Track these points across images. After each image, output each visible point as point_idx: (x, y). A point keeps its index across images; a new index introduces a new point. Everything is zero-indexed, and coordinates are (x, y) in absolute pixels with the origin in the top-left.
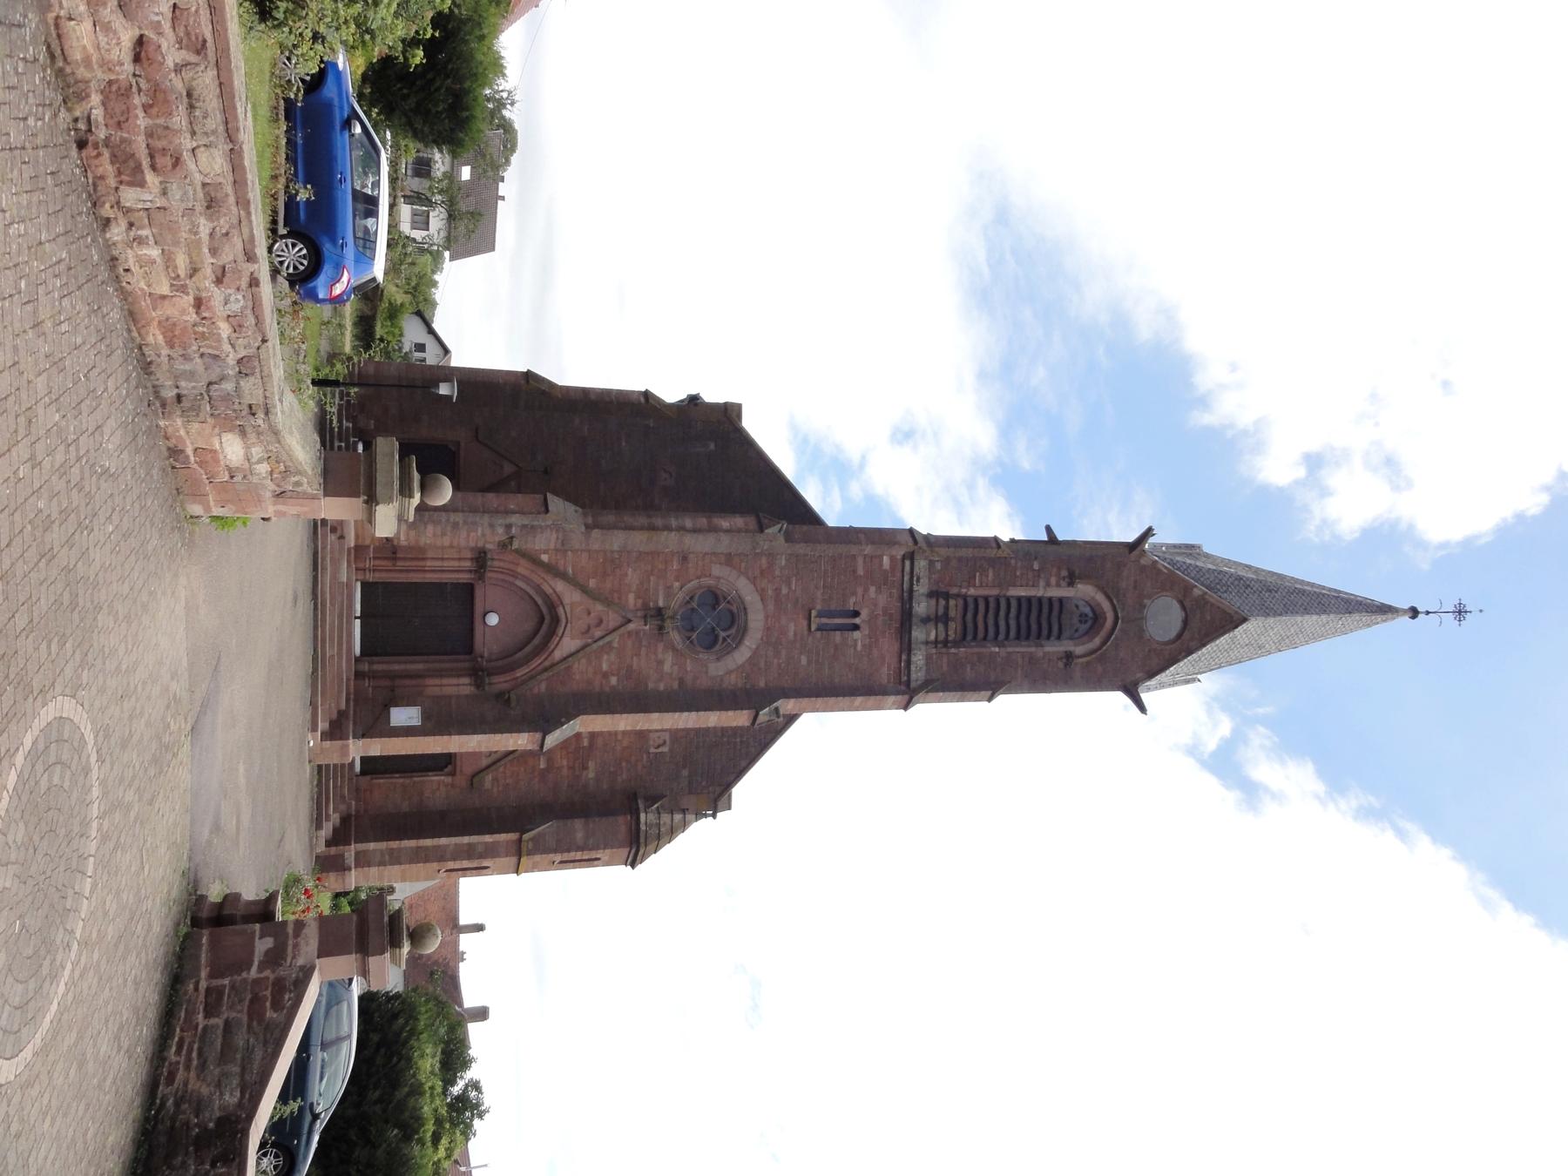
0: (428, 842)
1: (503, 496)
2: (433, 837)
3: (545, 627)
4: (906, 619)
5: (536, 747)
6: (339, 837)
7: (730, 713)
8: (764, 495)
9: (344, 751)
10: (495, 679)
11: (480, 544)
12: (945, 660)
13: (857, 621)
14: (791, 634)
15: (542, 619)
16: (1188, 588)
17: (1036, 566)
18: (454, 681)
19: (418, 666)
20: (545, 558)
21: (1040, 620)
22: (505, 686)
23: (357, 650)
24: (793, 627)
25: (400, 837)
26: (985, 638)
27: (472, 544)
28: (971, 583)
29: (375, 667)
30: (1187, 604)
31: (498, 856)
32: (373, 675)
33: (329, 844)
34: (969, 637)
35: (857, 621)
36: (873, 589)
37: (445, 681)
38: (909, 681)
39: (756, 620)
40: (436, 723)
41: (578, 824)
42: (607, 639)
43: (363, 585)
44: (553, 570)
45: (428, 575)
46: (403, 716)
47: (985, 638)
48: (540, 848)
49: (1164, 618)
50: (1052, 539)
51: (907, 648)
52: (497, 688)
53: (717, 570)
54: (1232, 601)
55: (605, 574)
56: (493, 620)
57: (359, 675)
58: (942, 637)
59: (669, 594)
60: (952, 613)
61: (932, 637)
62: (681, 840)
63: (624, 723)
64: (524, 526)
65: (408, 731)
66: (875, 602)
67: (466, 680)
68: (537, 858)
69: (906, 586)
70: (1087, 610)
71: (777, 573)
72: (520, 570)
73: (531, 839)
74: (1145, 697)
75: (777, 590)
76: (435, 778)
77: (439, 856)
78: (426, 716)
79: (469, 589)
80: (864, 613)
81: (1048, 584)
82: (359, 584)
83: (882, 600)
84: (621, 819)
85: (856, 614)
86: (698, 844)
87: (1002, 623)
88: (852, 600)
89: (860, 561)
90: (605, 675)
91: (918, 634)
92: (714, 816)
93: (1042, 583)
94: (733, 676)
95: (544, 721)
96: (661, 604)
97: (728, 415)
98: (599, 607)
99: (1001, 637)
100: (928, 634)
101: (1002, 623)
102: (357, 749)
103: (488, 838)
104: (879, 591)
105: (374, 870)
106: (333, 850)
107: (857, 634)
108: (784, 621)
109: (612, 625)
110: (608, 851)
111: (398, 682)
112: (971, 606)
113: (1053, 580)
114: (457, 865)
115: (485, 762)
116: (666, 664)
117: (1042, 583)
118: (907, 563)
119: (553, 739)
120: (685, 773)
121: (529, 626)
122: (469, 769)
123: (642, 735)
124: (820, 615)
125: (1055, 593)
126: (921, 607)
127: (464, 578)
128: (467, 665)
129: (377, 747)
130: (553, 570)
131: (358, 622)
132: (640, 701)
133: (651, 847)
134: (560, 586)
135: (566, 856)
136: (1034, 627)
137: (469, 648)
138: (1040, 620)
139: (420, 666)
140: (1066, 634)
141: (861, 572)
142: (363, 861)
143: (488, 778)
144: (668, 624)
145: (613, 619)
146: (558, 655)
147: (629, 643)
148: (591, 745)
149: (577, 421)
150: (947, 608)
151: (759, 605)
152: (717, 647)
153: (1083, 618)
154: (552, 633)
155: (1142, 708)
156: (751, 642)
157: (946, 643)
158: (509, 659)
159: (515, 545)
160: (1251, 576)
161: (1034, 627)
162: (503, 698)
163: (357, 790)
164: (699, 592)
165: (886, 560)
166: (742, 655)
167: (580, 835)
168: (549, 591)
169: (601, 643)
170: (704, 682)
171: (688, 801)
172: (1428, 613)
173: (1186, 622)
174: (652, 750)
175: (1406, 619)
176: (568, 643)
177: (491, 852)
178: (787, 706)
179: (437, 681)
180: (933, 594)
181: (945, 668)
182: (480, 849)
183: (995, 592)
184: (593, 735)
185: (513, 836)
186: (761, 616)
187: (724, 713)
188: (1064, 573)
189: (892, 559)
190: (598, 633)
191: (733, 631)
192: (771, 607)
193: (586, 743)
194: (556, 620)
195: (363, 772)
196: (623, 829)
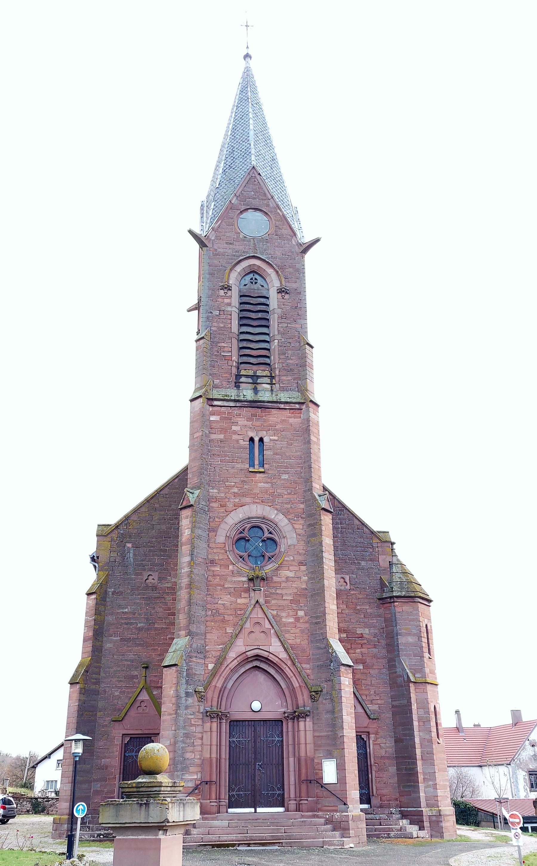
0: (418, 752)
1: (164, 699)
2: (411, 713)
3: (263, 665)
4: (255, 404)
5: (350, 671)
6: (417, 819)
7: (323, 528)
8: (167, 502)
9: (355, 819)
10: (300, 702)
11: (200, 716)
12: (284, 378)
13: (256, 439)
14: (266, 485)
15: (256, 667)
16: (231, 207)
17: (217, 313)
18: (302, 734)
19: (290, 764)
20: (211, 666)
21: (254, 312)
22: (306, 693)
23: (281, 809)
24: (260, 483)
25: (415, 774)
26: (269, 350)
27: (200, 722)
28: (230, 358)
29: (292, 795)
30: (243, 207)
31: (427, 699)
32: (299, 798)
33: (422, 828)
34: (267, 360)
35: (256, 439)
36: (234, 428)
37: (302, 741)
38: (299, 403)
39: (255, 510)
40: (333, 746)
41: (402, 640)
42: (270, 617)
43: (230, 807)
44: (220, 661)
45: (223, 756)
46: (329, 773)
47: (269, 350)
48: (420, 668)
49: (254, 224)
50: (197, 307)
51: (276, 405)
52: (309, 702)
53: (221, 538)
54: (241, 173)
55: (224, 621)
56: (256, 705)
57: (298, 809)
58: (268, 380)
59: (240, 574)
60: (251, 373)
61: (268, 386)
62: (410, 567)
63: (331, 606)
64: (187, 683)
65: (341, 769)
66: (244, 426)
67: (302, 724)
68: (427, 670)
69: (232, 404)
70: (248, 278)
71: (223, 495)
72: (219, 685)
73: (414, 675)
74: (307, 239)
75: (235, 495)
76: (372, 748)
77: (428, 743)
78: (329, 755)
79: (235, 724)
80: (251, 434)
81: (229, 304)
82: (231, 810)
83: (242, 421)
84: (398, 610)
85: (252, 440)
86: (416, 557)
87: (258, 338)
88: (241, 442)
89: (213, 436)
90: (297, 619)
91: (265, 396)
92: (393, 544)
93: (229, 309)
94: (296, 526)
95: (330, 663)
96: (245, 579)
97: (105, 533)
98: (247, 625)
99: (266, 338)
100: (265, 390)
101: (258, 338)
102: (355, 808)
103: (414, 707)
104: (236, 424)
105: (440, 793)
106: (427, 824)
107: (266, 440)
108: (257, 491)
109: (261, 615)
110: (421, 619)
111: (303, 777)
112: (245, 359)
113: (227, 301)
114: (434, 730)
115: (360, 710)
116: (290, 576)
117: (229, 309)
118: (216, 403)
119: (345, 659)
120: (363, 563)
121: (261, 677)
122: (365, 721)
123: (339, 594)
124: (252, 465)
125: (235, 300)
126: (248, 394)
127: (225, 727)
128: (290, 724)
129: (354, 793)
130: (220, 661)
131: (259, 810)
132: (317, 593)
133: (417, 588)
134: (232, 655)
135: (426, 650)
136: (260, 315)
137: (277, 723)
138: (254, 312)
139: (291, 760)
140: (265, 293)
141: (222, 436)
142: (433, 802)
143: (372, 707)
144: (262, 573)
145: (258, 614)
146: (283, 655)
147: (273, 602)
148: (345, 631)
149: (108, 645)
150: (247, 376)
151: (246, 508)
152: (276, 538)
153: (254, 281)
154: (267, 660)
155: (317, 241)
156: (272, 514)
157: (272, 377)
158: (287, 692)
159: (201, 689)
160: (222, 165)
161: (260, 315)
162: (315, 695)
163: (381, 807)
164: (237, 551)
165: (212, 418)
166: (282, 521)
167: (411, 639)
168: (235, 663)
169: (274, 624)
170: (301, 547)
171: (383, 560)
172: (247, 47)
173: (256, 209)
174: (348, 587)
175: (252, 63)
176: (275, 649)
177: (424, 704)
178: (317, 490)
179: (303, 747)
180: (237, 385)
181: (290, 378)
182: (422, 712)
183: (235, 341)
184: (340, 631)
185: (411, 685)
186: (254, 507)
187: (324, 533)
188: (222, 292)
189: (213, 414)
190: (268, 625)
191: (263, 526)
192: (247, 500)
193: (344, 635)
194: (258, 657)
195: (369, 802)
196: (407, 608)
